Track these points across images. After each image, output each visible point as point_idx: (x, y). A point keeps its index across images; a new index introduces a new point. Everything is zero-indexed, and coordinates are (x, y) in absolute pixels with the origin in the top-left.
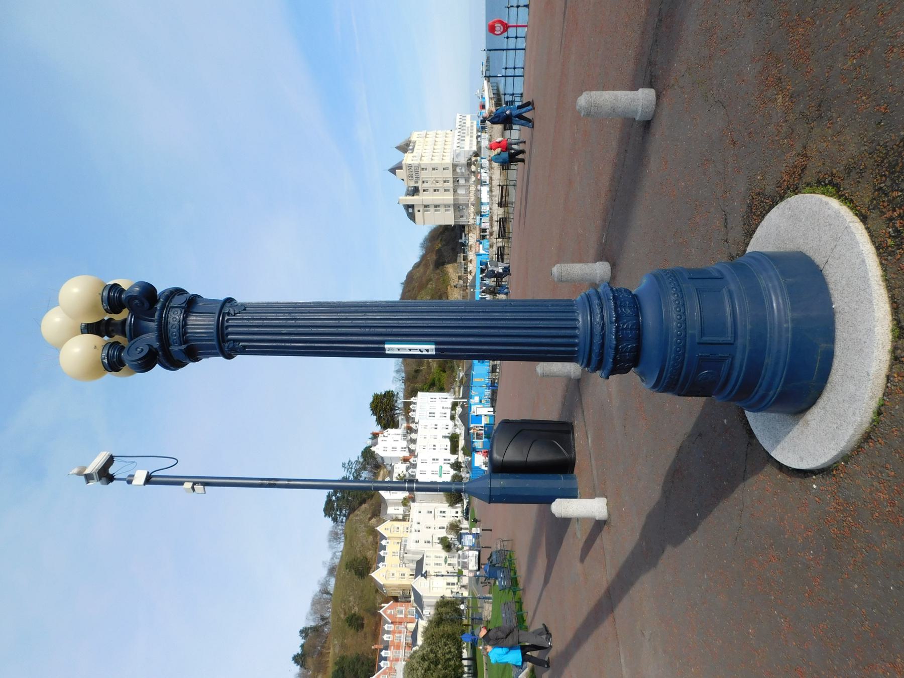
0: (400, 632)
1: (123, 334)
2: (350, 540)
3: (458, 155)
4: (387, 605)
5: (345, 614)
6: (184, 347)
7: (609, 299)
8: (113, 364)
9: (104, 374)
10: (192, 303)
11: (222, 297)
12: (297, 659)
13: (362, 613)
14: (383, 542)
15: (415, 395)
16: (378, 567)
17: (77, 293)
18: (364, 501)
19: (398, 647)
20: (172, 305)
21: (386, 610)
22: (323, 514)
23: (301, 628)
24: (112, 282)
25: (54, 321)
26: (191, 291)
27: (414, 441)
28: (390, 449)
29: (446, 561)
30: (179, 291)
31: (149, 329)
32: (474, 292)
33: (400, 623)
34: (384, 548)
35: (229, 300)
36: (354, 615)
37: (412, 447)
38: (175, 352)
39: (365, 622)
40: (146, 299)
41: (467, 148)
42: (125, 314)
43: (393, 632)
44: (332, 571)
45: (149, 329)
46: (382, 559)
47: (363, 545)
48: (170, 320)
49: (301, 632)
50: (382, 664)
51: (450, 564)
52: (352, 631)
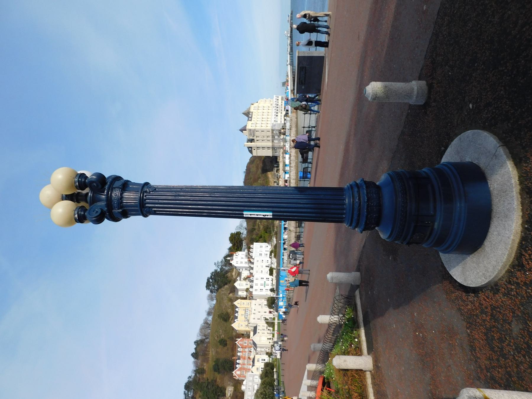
0: (245, 352)
1: (87, 202)
2: (219, 302)
3: (274, 125)
4: (239, 339)
5: (218, 337)
6: (120, 210)
7: (363, 189)
8: (81, 219)
9: (75, 224)
10: (126, 185)
11: (143, 182)
12: (193, 355)
13: (226, 338)
14: (237, 309)
15: (253, 244)
17: (60, 178)
18: (226, 284)
19: (244, 359)
20: (114, 186)
21: (239, 342)
23: (195, 340)
24: (82, 172)
25: (47, 193)
26: (125, 178)
27: (252, 268)
28: (239, 262)
30: (118, 178)
31: (100, 199)
32: (278, 320)
33: (245, 348)
34: (237, 312)
35: (147, 184)
37: (251, 271)
38: (116, 212)
40: (101, 182)
41: (279, 122)
42: (87, 190)
43: (242, 352)
44: (209, 314)
45: (100, 199)
46: (237, 318)
47: (226, 306)
48: (113, 195)
49: (195, 342)
50: (237, 366)
52: (221, 346)
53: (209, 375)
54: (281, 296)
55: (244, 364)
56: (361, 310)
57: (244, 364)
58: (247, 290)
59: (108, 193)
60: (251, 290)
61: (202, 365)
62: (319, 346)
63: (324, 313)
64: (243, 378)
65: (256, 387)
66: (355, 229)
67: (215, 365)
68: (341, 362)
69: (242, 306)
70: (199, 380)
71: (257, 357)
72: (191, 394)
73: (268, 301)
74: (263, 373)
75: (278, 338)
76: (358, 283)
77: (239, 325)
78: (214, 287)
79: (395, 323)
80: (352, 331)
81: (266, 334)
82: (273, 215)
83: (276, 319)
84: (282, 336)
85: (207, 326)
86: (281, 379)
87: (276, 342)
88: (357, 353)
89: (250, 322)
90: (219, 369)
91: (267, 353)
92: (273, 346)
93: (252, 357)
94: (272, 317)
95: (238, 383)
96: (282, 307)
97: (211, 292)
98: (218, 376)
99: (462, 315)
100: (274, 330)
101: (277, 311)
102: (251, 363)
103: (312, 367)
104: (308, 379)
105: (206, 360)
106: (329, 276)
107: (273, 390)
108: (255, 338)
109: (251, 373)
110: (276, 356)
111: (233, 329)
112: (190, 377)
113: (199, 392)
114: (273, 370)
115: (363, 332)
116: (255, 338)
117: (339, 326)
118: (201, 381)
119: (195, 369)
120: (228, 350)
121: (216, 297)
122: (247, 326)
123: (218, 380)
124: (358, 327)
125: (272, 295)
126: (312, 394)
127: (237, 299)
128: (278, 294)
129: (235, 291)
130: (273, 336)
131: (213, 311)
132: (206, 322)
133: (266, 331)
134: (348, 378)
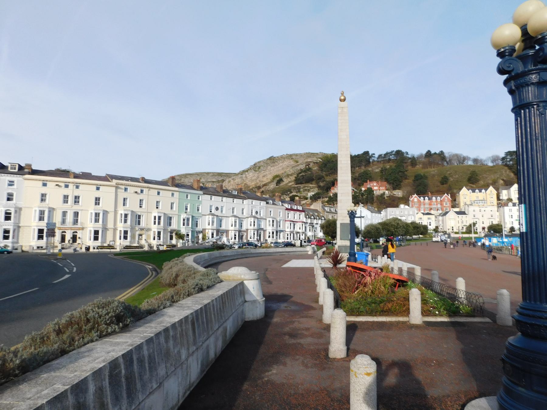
4: (449, 197)
5: (449, 174)
16: (468, 190)
19: (430, 204)
21: (447, 197)
22: (506, 151)
23: (444, 151)
29: (464, 226)
32: (475, 238)
33: (441, 204)
34: (480, 191)
36: (448, 179)
39: (445, 186)
44: (475, 160)
46: (474, 191)
47: (486, 178)
49: (442, 152)
50: (422, 198)
51: (463, 228)
52: (440, 179)
53: (411, 171)
54: (505, 240)
55: (424, 205)
56: (468, 321)
57: (424, 205)
58: (510, 200)
59: (533, 70)
60: (510, 204)
61: (420, 163)
62: (436, 279)
63: (467, 285)
64: (410, 205)
65: (403, 218)
66: (517, 312)
67: (421, 176)
68: (415, 297)
69: (488, 196)
70: (406, 163)
71: (433, 217)
72: (392, 157)
73: (498, 225)
74: (417, 224)
75: (454, 238)
76: (498, 321)
77: (465, 195)
78: (510, 161)
79: (450, 347)
80: (447, 310)
81: (458, 225)
82: (523, 233)
83: (476, 235)
84: (457, 242)
85: (462, 161)
86: (412, 243)
87: (449, 236)
88: (424, 311)
89: (470, 207)
90: (417, 180)
91: (437, 227)
92: (445, 233)
93: (432, 212)
94: (478, 231)
95: (406, 201)
96: (490, 241)
97: (503, 159)
98: (410, 181)
99: (444, 396)
100: (463, 233)
101: (486, 236)
102: (426, 212)
103: (418, 271)
104: (408, 268)
105: (426, 165)
106: (505, 292)
107: (402, 235)
108: (452, 214)
109: (416, 212)
110: (435, 237)
111: (460, 189)
112: (407, 153)
113: (395, 165)
114: (421, 234)
115: (445, 319)
116: (452, 214)
117: (454, 298)
118: (405, 165)
119: (415, 156)
120: (437, 186)
121: (497, 165)
122: (466, 204)
123: (407, 181)
124: (450, 316)
125: (506, 230)
126: (396, 272)
127: (497, 189)
128: (507, 236)
129: (507, 185)
130: (456, 233)
131: (479, 164)
132: (465, 159)
133: (461, 225)
134: (402, 301)
